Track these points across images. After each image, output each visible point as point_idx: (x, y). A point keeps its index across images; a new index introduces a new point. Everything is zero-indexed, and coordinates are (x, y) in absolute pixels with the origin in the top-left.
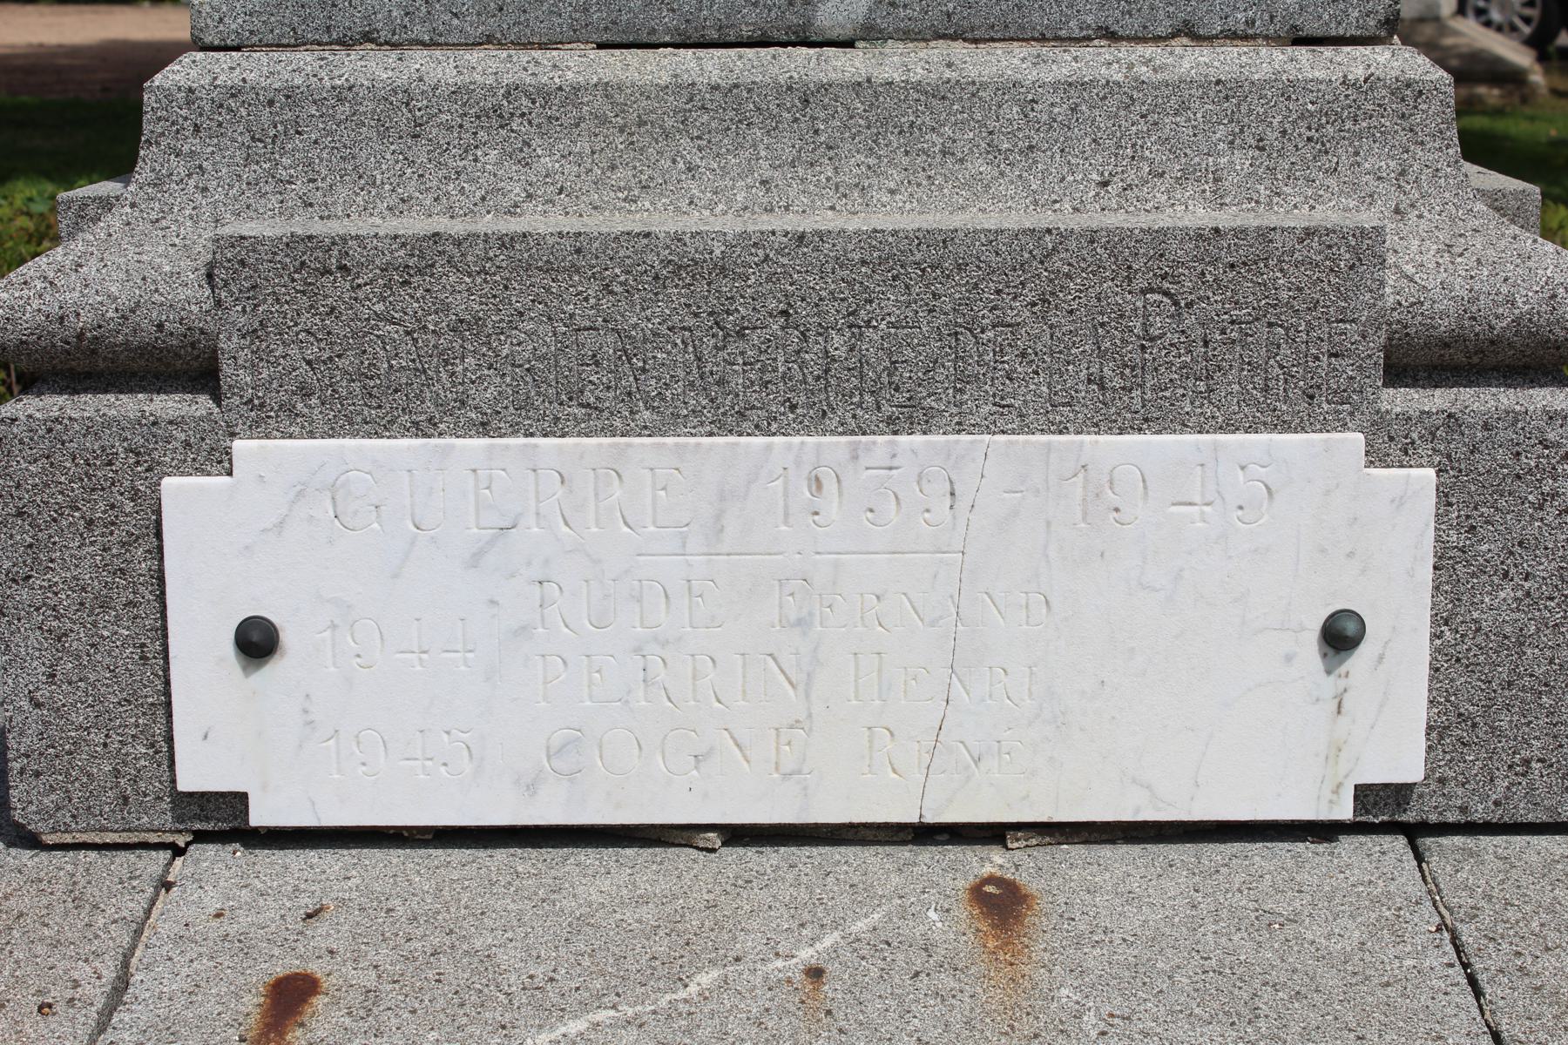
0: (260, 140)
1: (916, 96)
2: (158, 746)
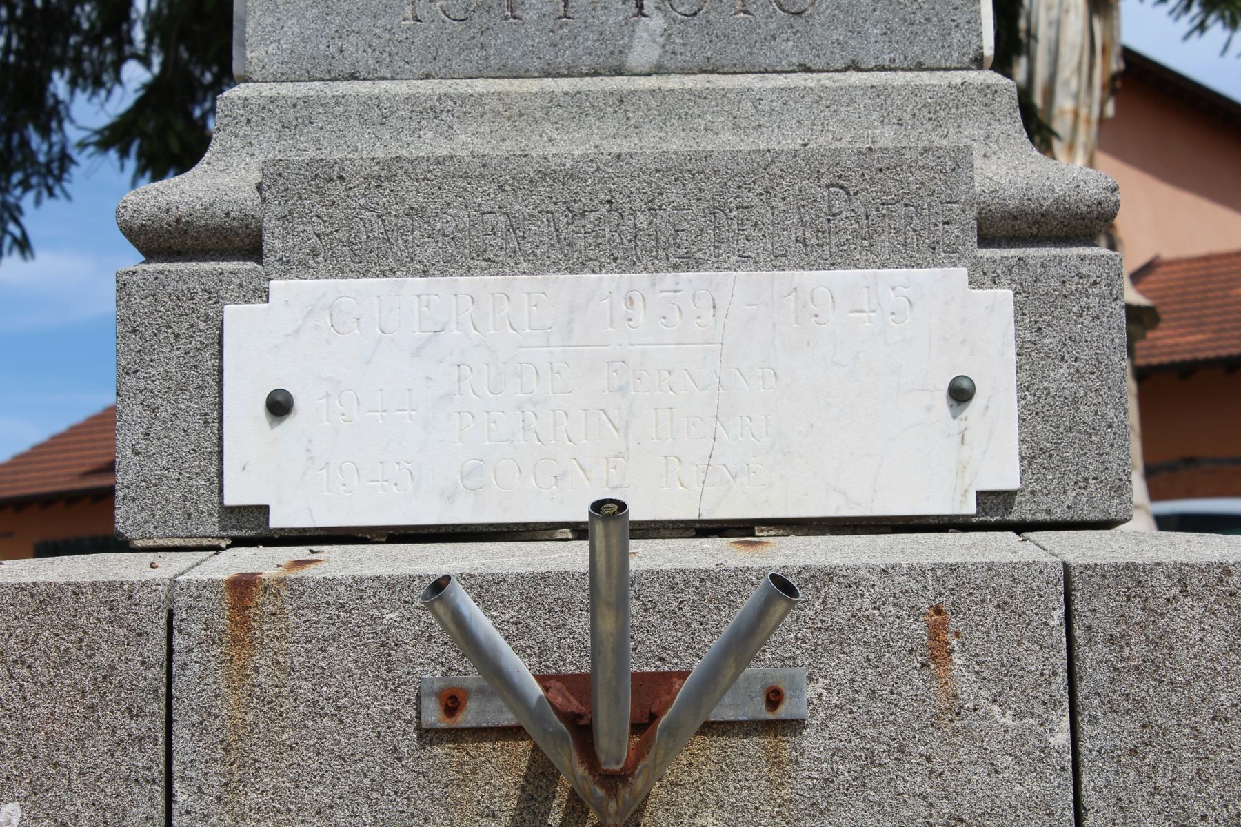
0: (287, 127)
1: (688, 97)
2: (212, 479)
